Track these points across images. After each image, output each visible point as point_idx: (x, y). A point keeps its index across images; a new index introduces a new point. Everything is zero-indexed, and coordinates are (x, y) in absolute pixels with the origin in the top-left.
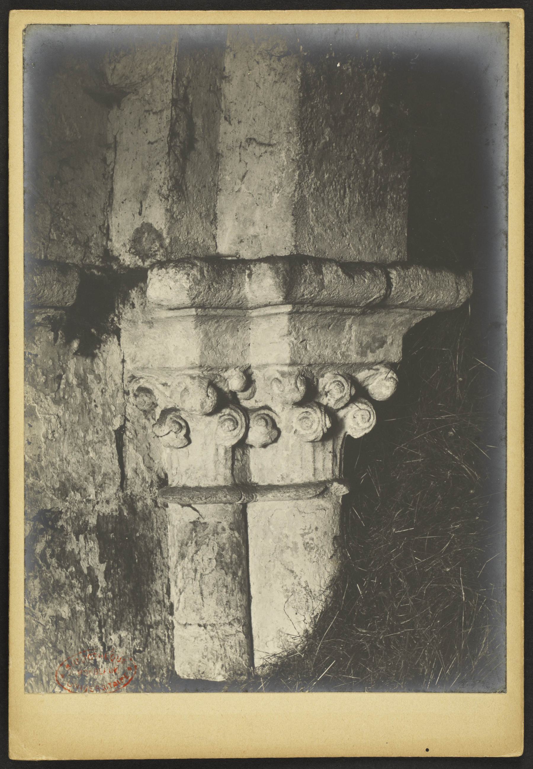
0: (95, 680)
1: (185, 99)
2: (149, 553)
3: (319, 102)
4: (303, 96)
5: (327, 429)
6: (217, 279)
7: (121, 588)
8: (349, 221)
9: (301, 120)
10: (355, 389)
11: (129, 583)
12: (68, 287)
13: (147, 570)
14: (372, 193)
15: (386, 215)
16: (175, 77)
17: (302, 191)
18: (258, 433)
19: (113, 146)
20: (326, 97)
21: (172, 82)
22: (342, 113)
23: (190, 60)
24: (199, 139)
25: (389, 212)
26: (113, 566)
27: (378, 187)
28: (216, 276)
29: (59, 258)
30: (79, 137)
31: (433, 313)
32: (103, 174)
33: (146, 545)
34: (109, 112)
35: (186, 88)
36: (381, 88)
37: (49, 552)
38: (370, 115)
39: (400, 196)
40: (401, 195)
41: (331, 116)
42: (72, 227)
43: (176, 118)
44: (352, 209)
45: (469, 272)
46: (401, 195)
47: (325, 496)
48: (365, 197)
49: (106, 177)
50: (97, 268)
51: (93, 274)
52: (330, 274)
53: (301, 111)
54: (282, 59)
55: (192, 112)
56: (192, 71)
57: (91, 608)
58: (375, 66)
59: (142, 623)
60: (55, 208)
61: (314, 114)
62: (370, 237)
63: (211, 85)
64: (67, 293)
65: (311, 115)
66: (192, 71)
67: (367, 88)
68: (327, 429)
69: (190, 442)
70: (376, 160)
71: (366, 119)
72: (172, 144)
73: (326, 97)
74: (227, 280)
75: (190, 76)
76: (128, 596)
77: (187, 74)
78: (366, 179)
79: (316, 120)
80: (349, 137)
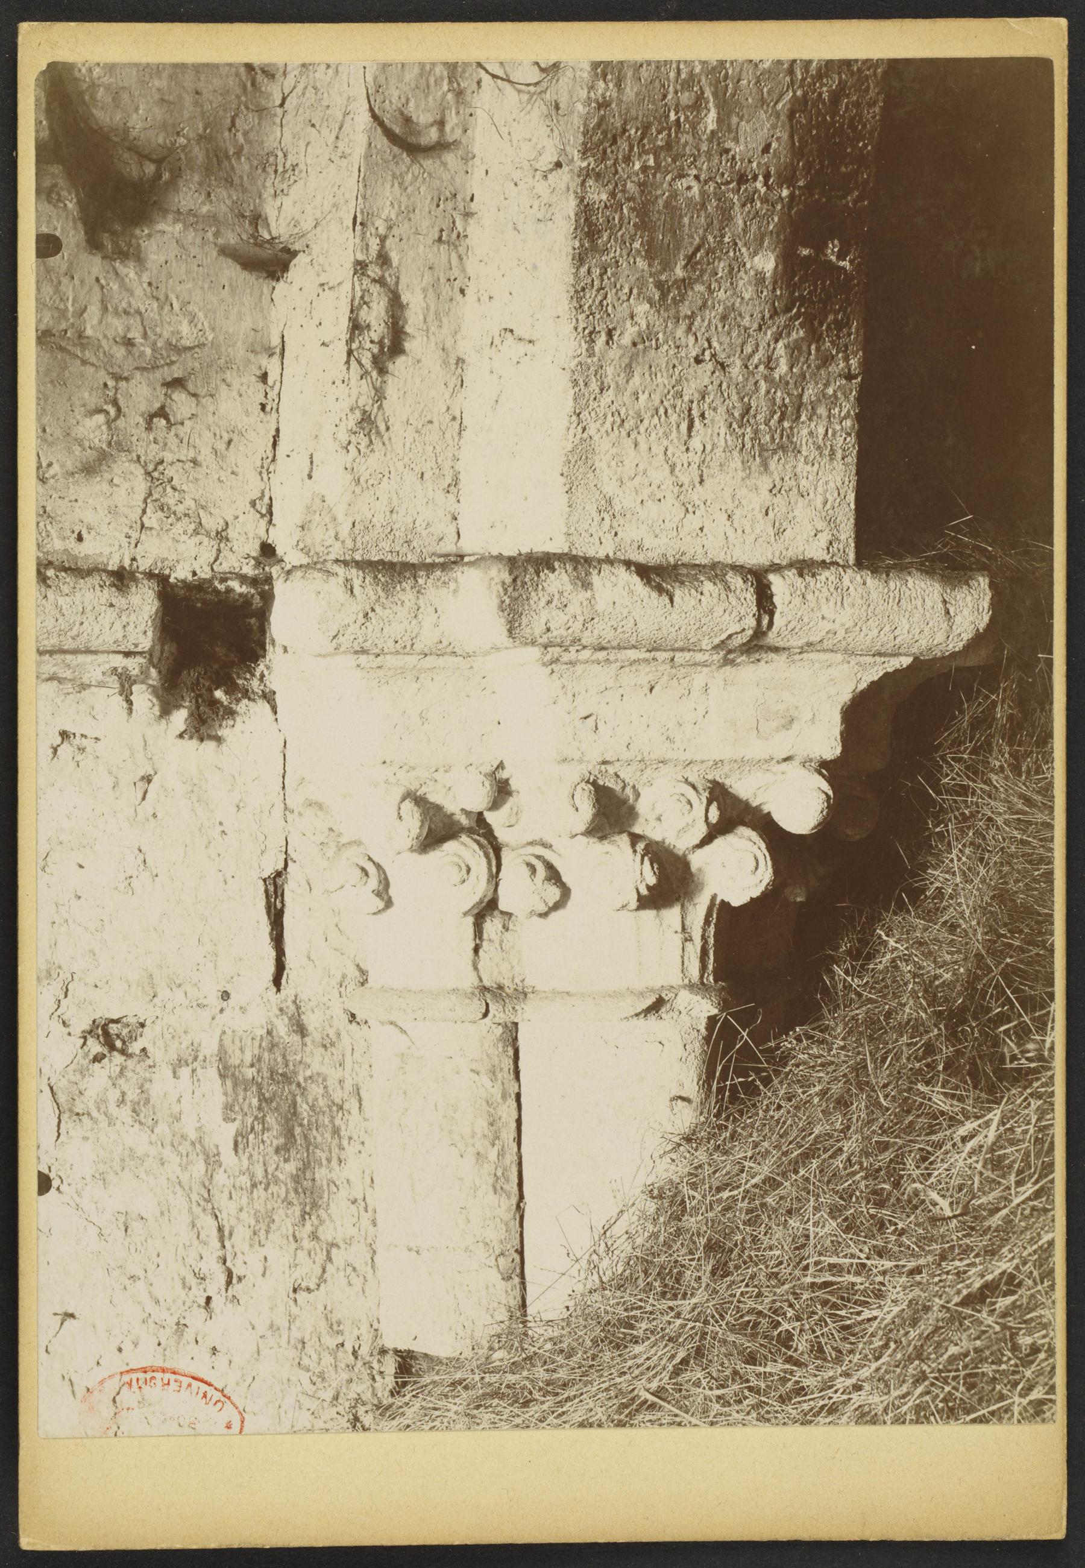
0: (922, 1290)
1: (383, 259)
2: (335, 1108)
3: (621, 256)
4: (582, 246)
5: (648, 887)
6: (383, 600)
7: (270, 1170)
8: (701, 482)
9: (576, 292)
10: (719, 808)
11: (286, 1160)
12: (133, 617)
13: (329, 1140)
14: (762, 427)
15: (799, 469)
16: (359, 220)
17: (584, 429)
18: (519, 890)
19: (278, 351)
20: (637, 245)
21: (354, 230)
22: (679, 272)
23: (392, 186)
24: (416, 334)
25: (806, 463)
26: (253, 1128)
27: (775, 412)
28: (382, 594)
29: (162, 562)
30: (210, 338)
31: (906, 661)
32: (261, 404)
33: (327, 1094)
34: (274, 288)
35: (383, 239)
36: (776, 219)
37: (114, 1095)
38: (752, 273)
39: (834, 430)
40: (838, 427)
41: (651, 280)
42: (192, 504)
43: (362, 297)
44: (708, 459)
45: (981, 579)
46: (838, 427)
47: (664, 1016)
48: (744, 435)
49: (268, 408)
50: (243, 579)
51: (229, 590)
52: (617, 590)
53: (576, 274)
54: (550, 176)
55: (397, 283)
56: (396, 207)
57: (202, 1203)
58: (761, 178)
59: (314, 1236)
60: (155, 469)
61: (609, 279)
62: (755, 512)
63: (442, 230)
64: (132, 625)
65: (602, 280)
66: (396, 207)
67: (740, 222)
68: (648, 887)
69: (389, 903)
70: (770, 363)
71: (741, 283)
72: (354, 346)
73: (637, 245)
74: (406, 601)
75: (393, 216)
76: (286, 1185)
77: (386, 211)
78: (746, 400)
79: (614, 291)
80: (699, 318)
